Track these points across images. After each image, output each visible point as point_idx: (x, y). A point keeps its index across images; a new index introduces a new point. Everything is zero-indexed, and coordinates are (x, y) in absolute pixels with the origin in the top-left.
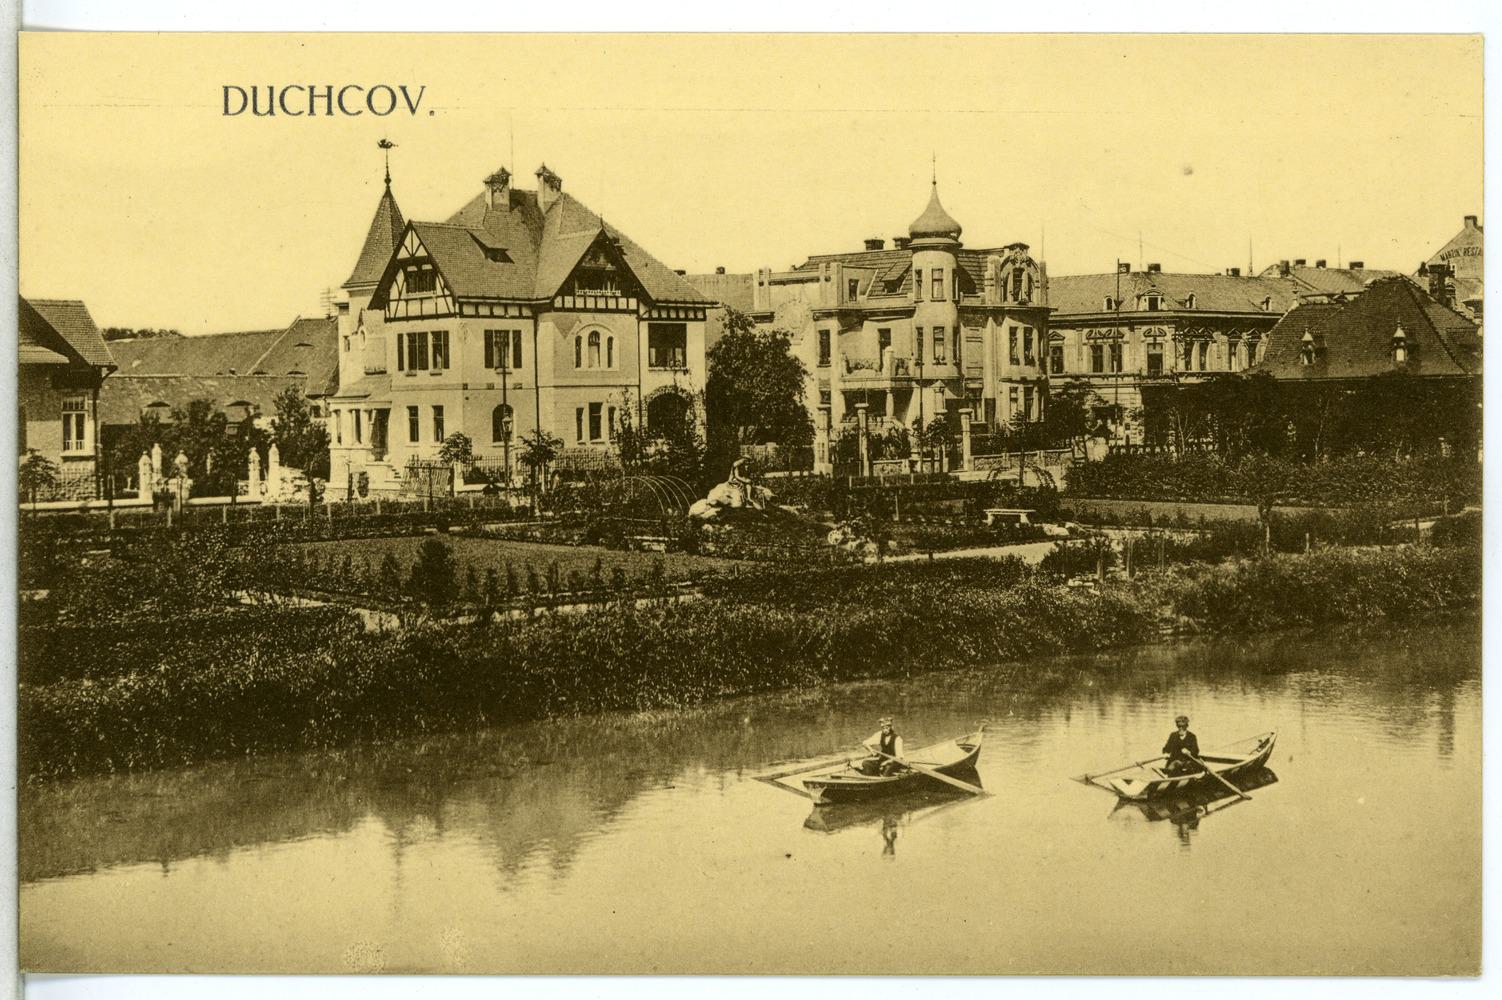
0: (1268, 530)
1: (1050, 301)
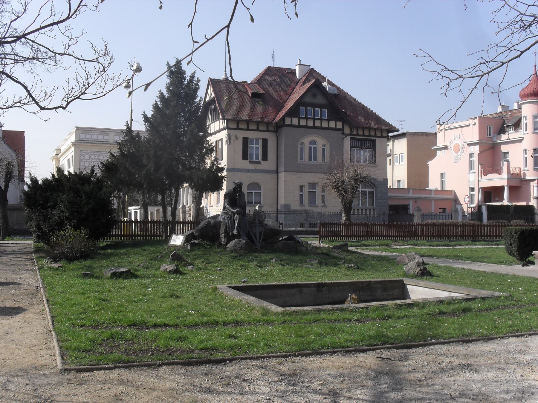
0: (487, 204)
1: (20, 43)
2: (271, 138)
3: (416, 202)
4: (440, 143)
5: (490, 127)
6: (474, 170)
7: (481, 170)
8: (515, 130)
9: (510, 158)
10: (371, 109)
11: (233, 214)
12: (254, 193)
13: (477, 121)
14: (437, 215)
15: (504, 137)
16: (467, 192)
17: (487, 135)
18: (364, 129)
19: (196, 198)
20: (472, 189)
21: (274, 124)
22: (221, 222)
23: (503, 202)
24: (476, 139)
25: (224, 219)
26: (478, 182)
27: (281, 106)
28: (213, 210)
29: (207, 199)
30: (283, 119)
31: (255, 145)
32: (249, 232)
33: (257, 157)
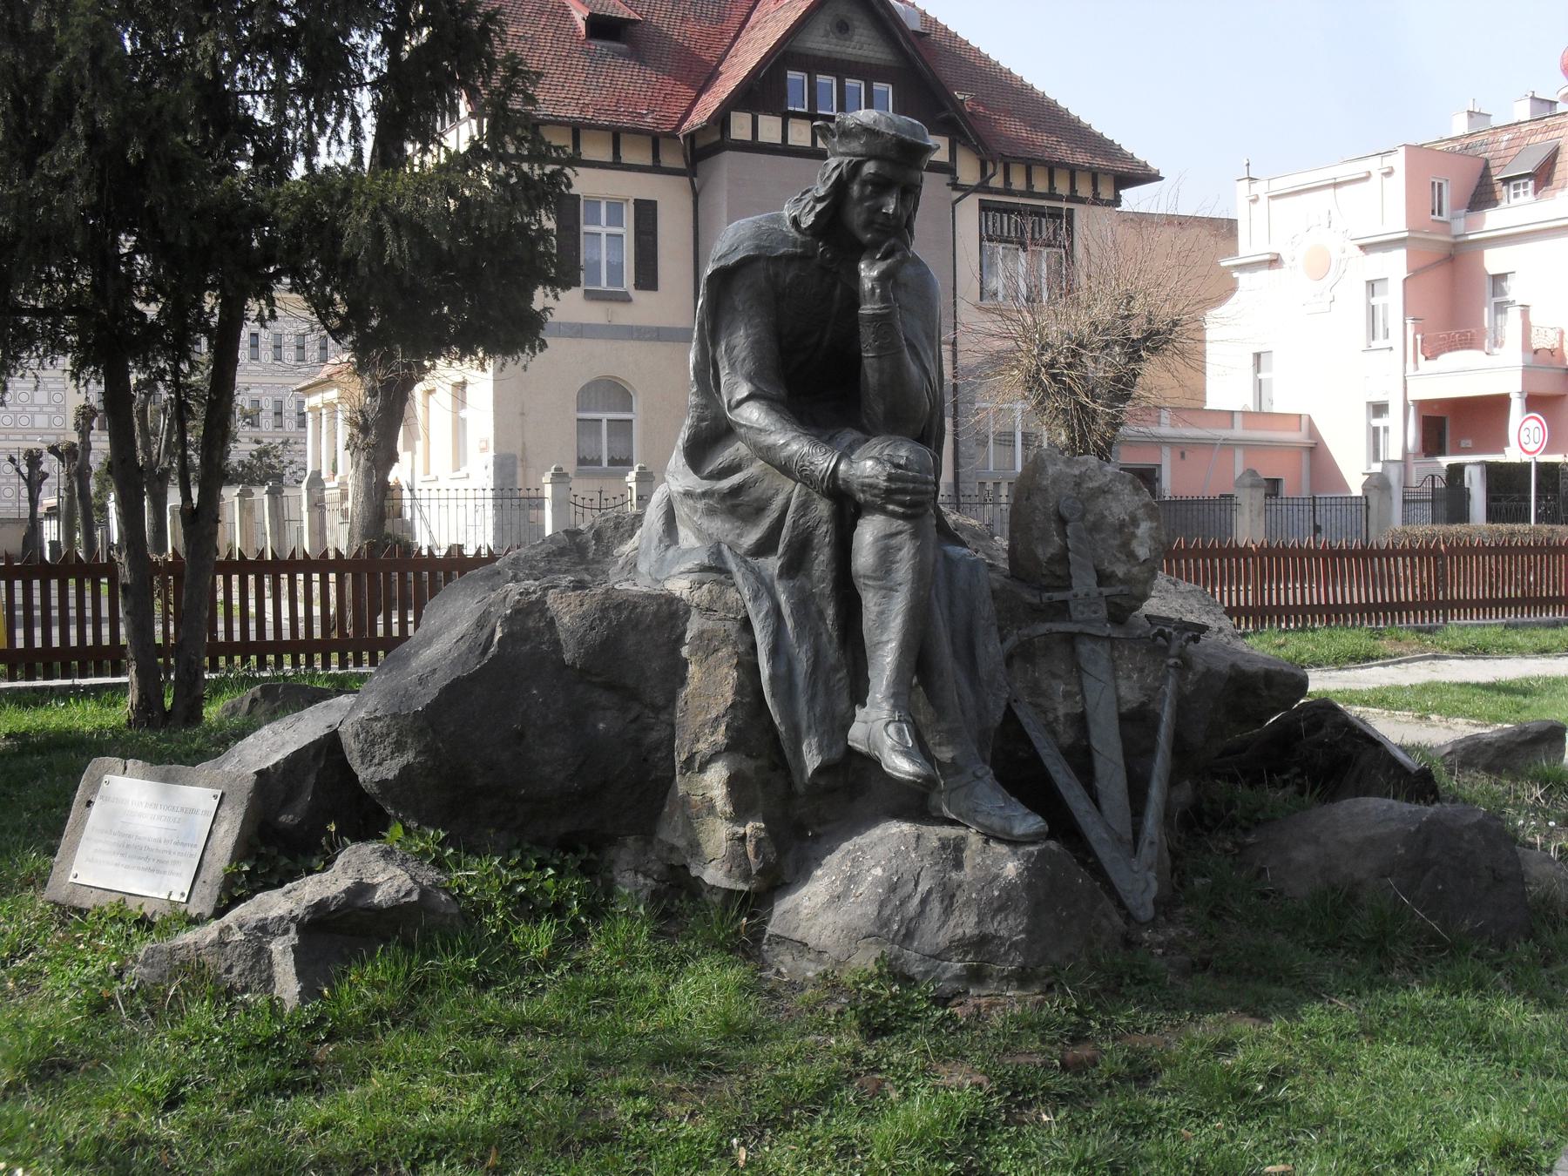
2: (670, 196)
3: (1183, 455)
4: (1249, 245)
5: (1440, 185)
6: (1387, 336)
7: (1415, 340)
8: (1536, 193)
9: (1515, 291)
10: (1051, 95)
11: (822, 508)
12: (604, 424)
13: (1399, 161)
14: (1317, 501)
15: (1493, 220)
16: (1360, 420)
17: (1433, 213)
18: (1029, 165)
19: (364, 429)
20: (1379, 409)
21: (685, 137)
22: (671, 613)
23: (1503, 452)
24: (1396, 222)
25: (716, 569)
26: (1405, 382)
27: (707, 77)
28: (471, 494)
29: (414, 453)
30: (721, 119)
31: (609, 224)
32: (1010, 715)
33: (616, 271)
